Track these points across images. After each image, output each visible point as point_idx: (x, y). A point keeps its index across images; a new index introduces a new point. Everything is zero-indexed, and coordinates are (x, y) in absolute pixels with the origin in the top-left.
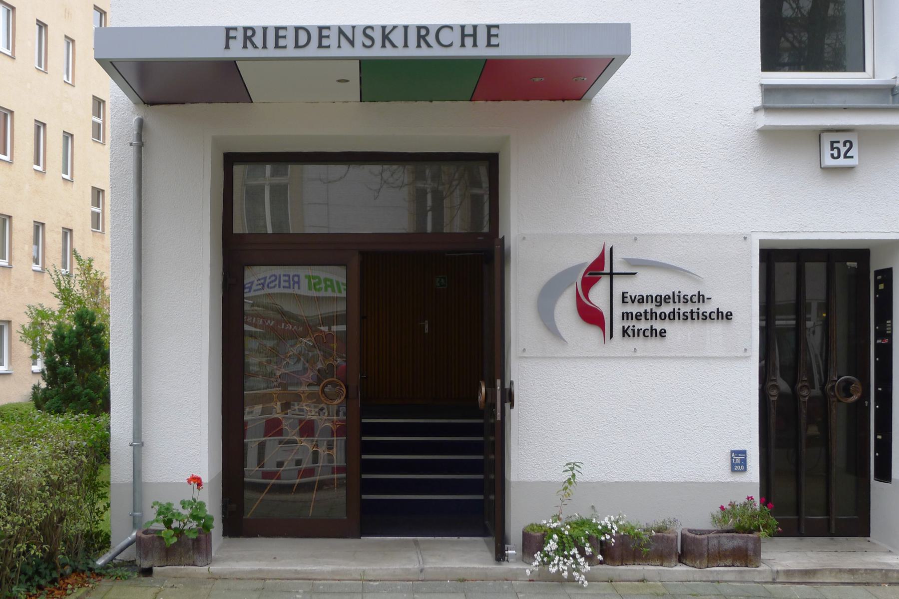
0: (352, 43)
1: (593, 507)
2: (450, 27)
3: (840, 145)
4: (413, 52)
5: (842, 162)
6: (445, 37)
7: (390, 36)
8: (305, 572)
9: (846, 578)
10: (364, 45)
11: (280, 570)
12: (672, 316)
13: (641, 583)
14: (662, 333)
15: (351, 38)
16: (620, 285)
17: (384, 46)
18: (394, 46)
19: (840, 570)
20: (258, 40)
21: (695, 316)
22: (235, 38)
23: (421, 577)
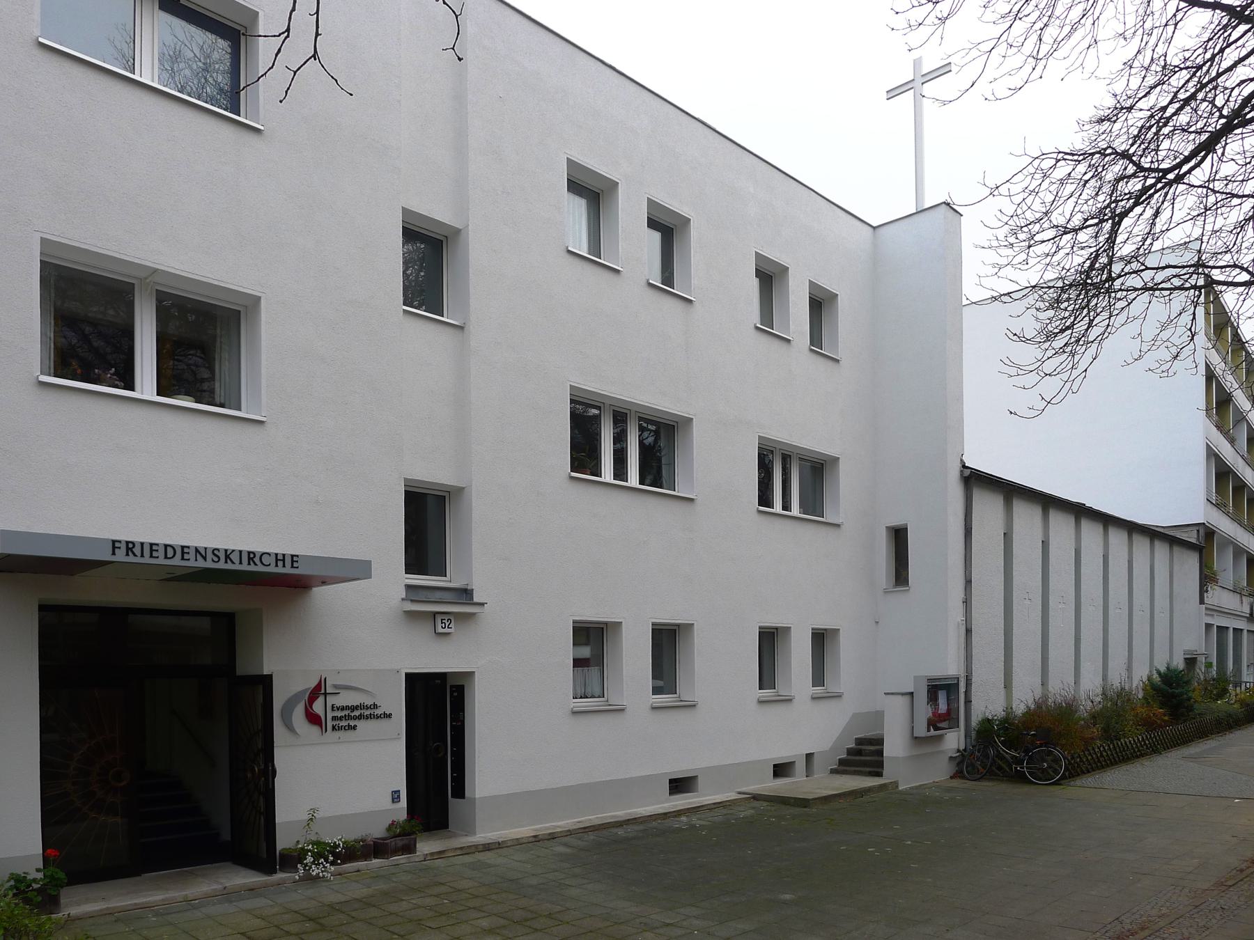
0: (205, 558)
1: (317, 833)
2: (269, 554)
4: (245, 567)
5: (446, 630)
6: (266, 560)
7: (230, 556)
8: (143, 903)
9: (464, 851)
10: (213, 560)
11: (122, 906)
12: (360, 717)
13: (358, 873)
14: (355, 728)
15: (198, 554)
16: (331, 700)
17: (226, 562)
18: (233, 563)
19: (456, 849)
20: (137, 550)
21: (372, 716)
22: (120, 548)
23: (225, 892)
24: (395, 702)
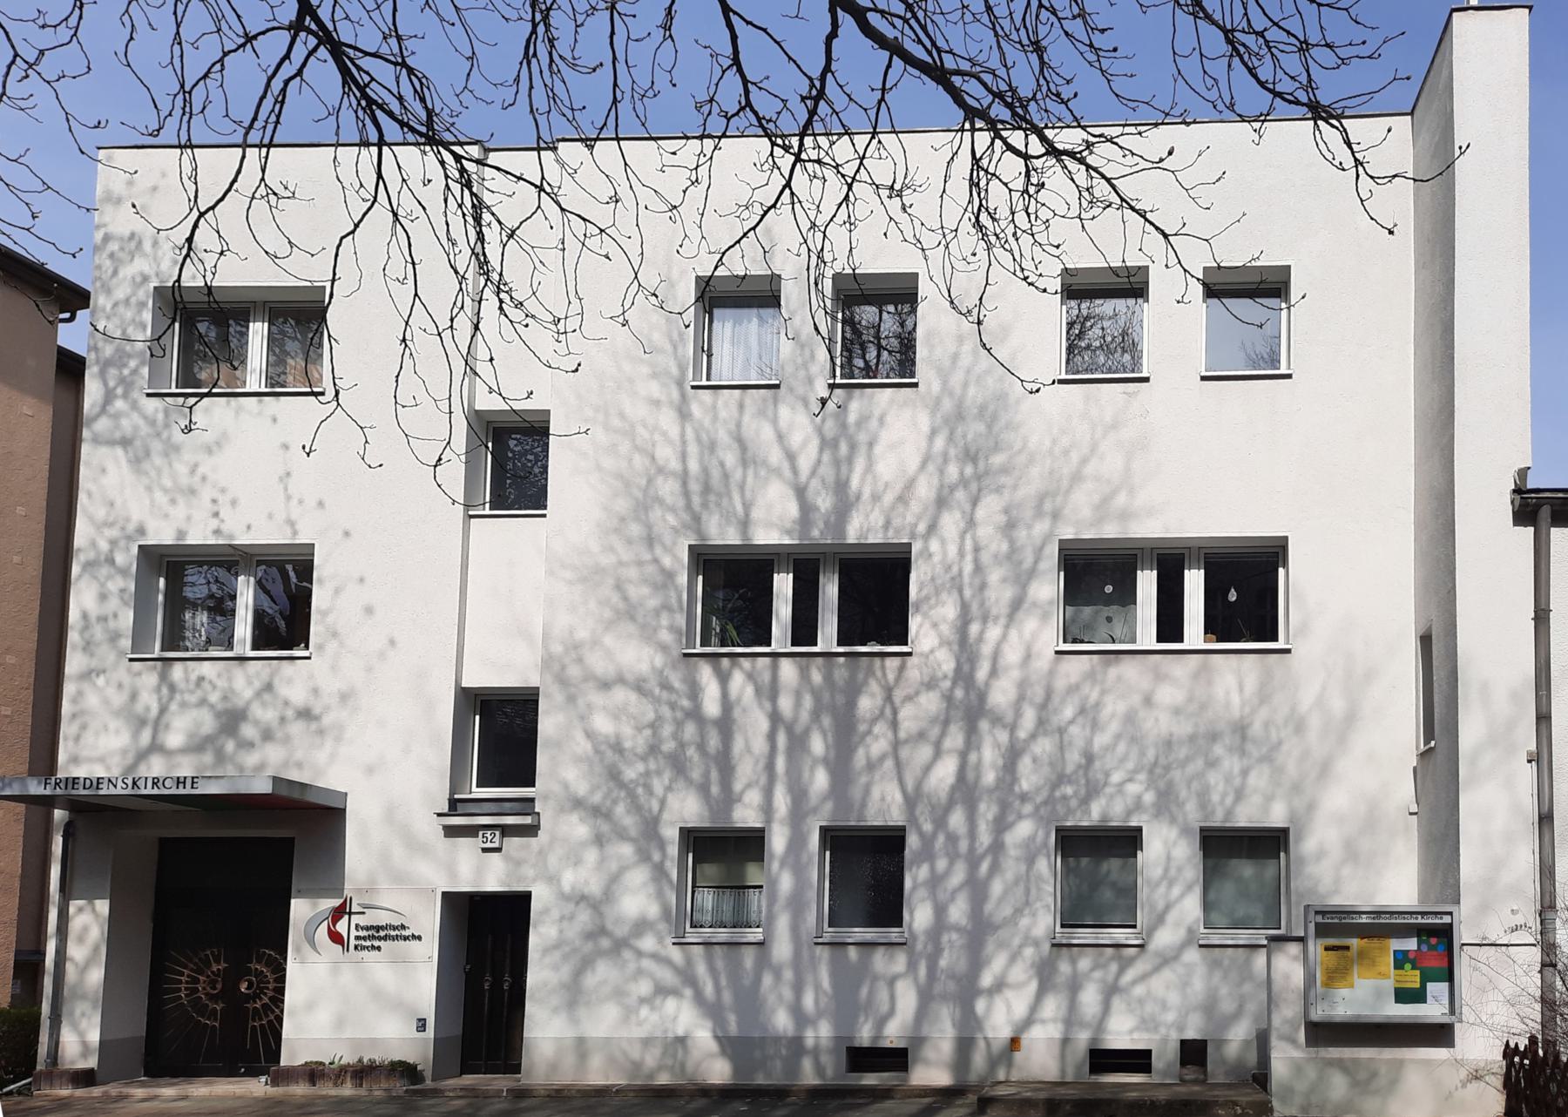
0: (115, 786)
3: (488, 835)
12: (385, 938)
16: (355, 919)
24: (428, 921)
